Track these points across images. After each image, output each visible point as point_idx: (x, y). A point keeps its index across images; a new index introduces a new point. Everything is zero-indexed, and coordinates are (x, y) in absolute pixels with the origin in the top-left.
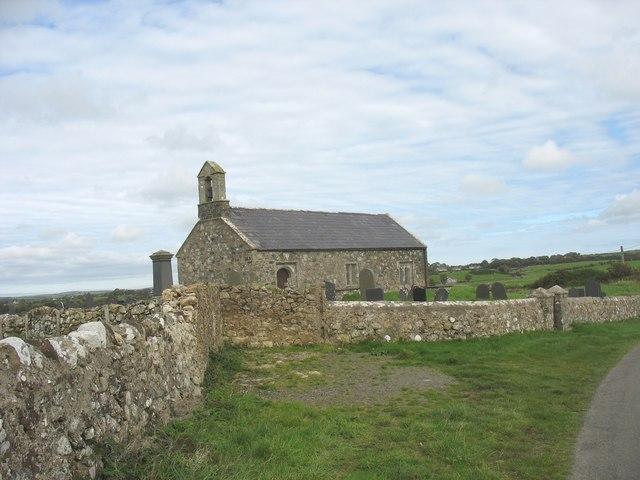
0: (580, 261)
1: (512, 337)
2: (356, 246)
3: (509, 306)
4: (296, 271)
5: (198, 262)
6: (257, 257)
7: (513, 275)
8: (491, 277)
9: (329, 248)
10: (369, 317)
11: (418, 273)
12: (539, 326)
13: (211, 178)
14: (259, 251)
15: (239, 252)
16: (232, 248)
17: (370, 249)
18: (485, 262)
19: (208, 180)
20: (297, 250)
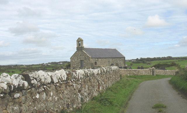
0: (171, 59)
1: (145, 75)
2: (110, 57)
3: (144, 70)
5: (76, 60)
6: (91, 59)
7: (147, 64)
8: (140, 64)
10: (121, 71)
12: (149, 74)
13: (80, 41)
17: (113, 58)
18: (137, 59)
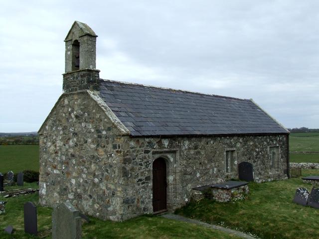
4: (175, 161)
5: (59, 143)
9: (240, 132)
11: (282, 157)
14: (131, 137)
15: (219, 151)
16: (98, 131)
19: (76, 44)
20: (179, 136)
